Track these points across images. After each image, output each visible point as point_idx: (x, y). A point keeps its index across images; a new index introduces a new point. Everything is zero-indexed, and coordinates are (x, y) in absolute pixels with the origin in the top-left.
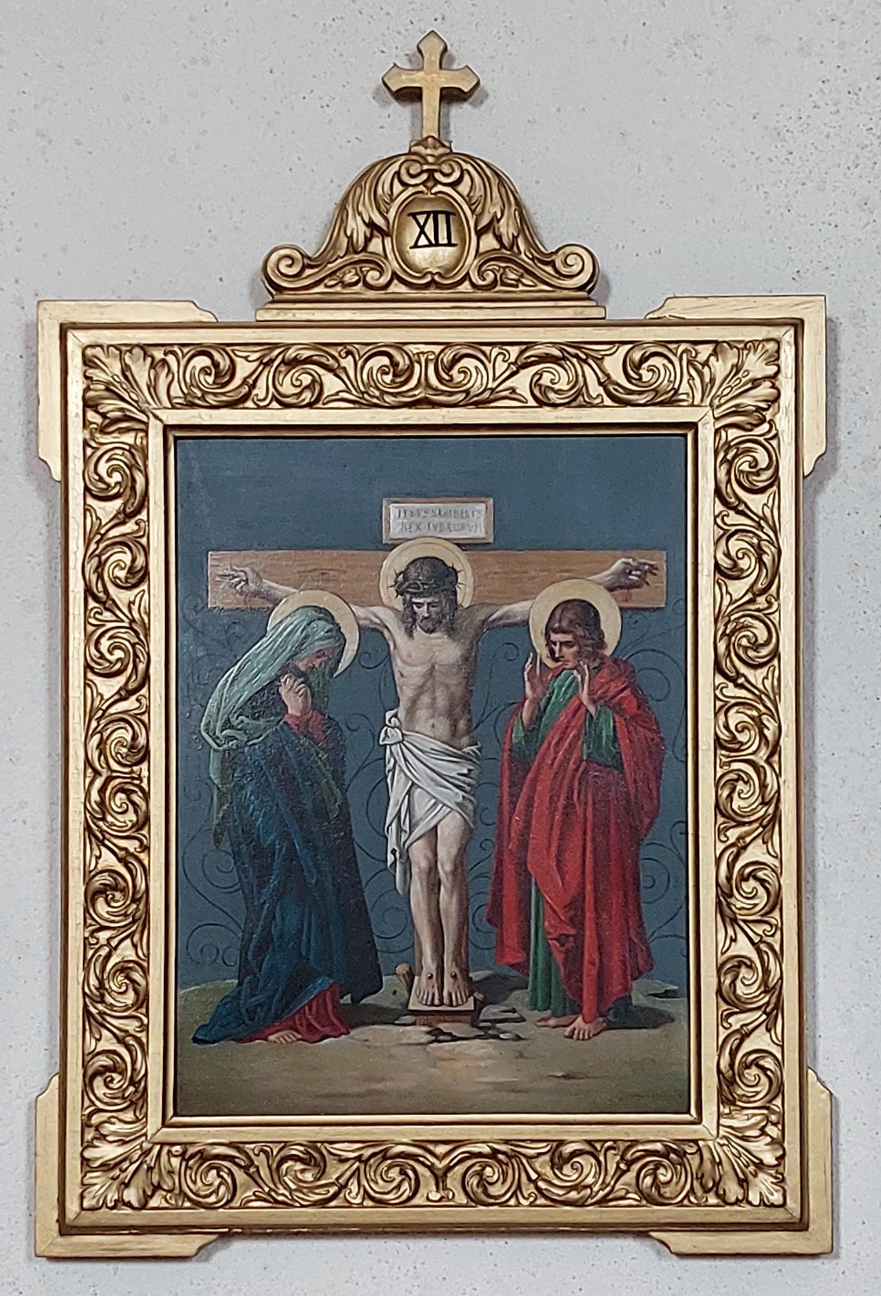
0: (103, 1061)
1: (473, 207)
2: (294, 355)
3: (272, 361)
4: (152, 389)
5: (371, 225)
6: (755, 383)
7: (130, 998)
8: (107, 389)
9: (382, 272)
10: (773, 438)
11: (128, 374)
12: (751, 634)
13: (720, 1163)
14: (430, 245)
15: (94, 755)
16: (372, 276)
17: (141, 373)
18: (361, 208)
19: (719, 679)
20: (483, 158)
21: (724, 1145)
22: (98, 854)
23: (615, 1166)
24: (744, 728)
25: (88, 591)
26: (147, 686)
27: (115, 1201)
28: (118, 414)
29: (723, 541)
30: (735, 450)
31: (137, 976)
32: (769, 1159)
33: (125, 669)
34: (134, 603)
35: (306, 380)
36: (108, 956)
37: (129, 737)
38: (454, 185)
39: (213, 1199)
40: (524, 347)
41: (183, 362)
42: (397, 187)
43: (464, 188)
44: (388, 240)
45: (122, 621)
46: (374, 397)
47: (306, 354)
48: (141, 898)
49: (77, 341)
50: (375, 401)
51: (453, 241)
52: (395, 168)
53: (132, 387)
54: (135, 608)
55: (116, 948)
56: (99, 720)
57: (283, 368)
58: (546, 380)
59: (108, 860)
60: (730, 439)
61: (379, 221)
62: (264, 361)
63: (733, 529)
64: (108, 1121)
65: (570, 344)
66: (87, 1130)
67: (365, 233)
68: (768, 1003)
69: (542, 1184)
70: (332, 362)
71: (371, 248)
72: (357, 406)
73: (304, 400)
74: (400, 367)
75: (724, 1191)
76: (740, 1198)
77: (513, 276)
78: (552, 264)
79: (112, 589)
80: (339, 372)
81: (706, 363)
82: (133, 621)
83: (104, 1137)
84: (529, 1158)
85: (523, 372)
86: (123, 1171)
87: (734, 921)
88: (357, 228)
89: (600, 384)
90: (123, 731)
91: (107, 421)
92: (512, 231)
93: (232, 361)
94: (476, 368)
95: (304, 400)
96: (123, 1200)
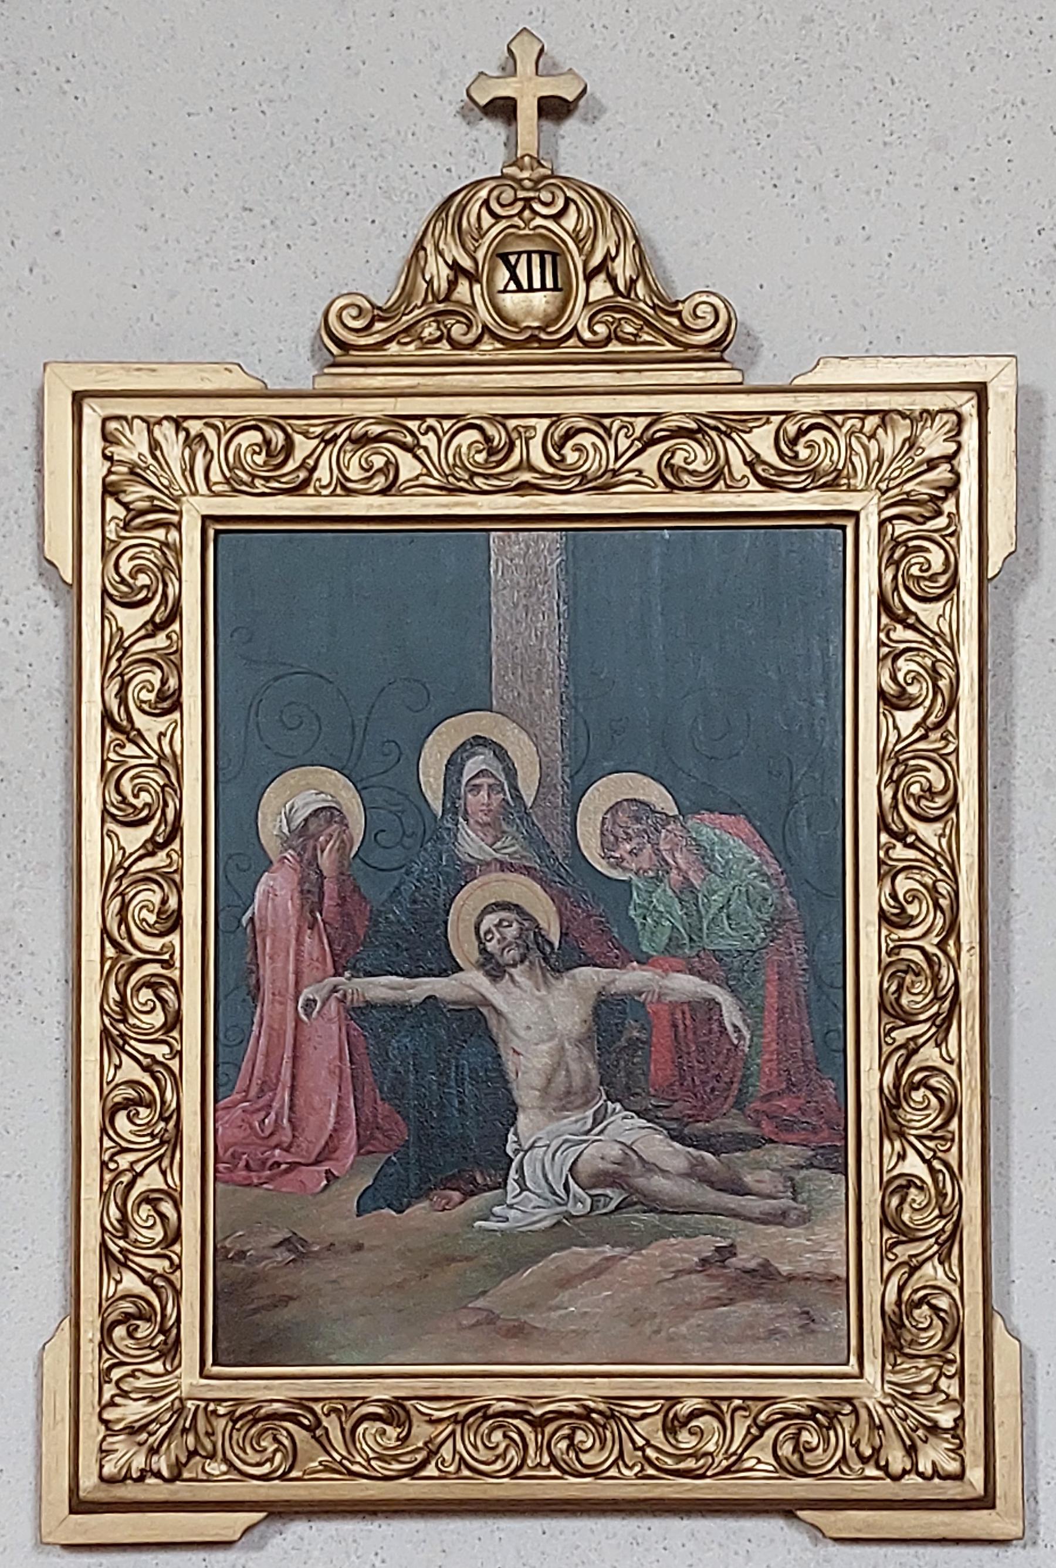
0: (127, 1306)
1: (581, 245)
2: (364, 430)
3: (336, 437)
4: (187, 474)
5: (455, 267)
6: (932, 464)
7: (158, 1019)
8: (132, 472)
9: (469, 326)
10: (951, 535)
11: (158, 453)
12: (923, 780)
13: (881, 1427)
14: (520, 289)
15: (113, 925)
16: (457, 331)
17: (173, 448)
18: (441, 246)
19: (884, 838)
20: (590, 183)
21: (889, 1406)
22: (118, 1063)
23: (744, 1432)
24: (914, 897)
25: (107, 716)
26: (178, 840)
27: (142, 1470)
28: (146, 504)
29: (889, 662)
30: (903, 549)
31: (168, 994)
32: (946, 1419)
33: (152, 818)
34: (165, 735)
35: (379, 462)
36: (131, 1184)
37: (157, 899)
38: (557, 217)
39: (266, 1469)
40: (655, 417)
41: (225, 439)
42: (487, 220)
43: (570, 221)
44: (477, 288)
45: (149, 757)
46: (459, 480)
47: (377, 429)
48: (171, 1116)
49: (92, 415)
50: (462, 484)
51: (560, 286)
52: (483, 194)
53: (163, 469)
54: (165, 742)
55: (141, 1174)
56: (121, 878)
57: (349, 447)
58: (678, 460)
59: (131, 1070)
60: (896, 534)
61: (466, 263)
62: (327, 437)
63: (902, 646)
64: (132, 1375)
65: (711, 415)
66: (106, 1386)
67: (448, 276)
68: (943, 1230)
69: (649, 1452)
70: (409, 439)
71: (455, 296)
72: (444, 493)
73: (375, 485)
74: (495, 443)
75: (887, 1462)
76: (908, 1467)
77: (629, 329)
78: (678, 315)
79: (141, 721)
80: (420, 452)
81: (872, 436)
82: (162, 757)
83: (125, 1394)
84: (631, 1419)
85: (651, 450)
86: (151, 1434)
87: (902, 1135)
88: (438, 271)
89: (746, 463)
90: (150, 893)
91: (132, 513)
92: (630, 272)
93: (288, 438)
94: (593, 444)
95: (375, 485)
96: (151, 1470)
